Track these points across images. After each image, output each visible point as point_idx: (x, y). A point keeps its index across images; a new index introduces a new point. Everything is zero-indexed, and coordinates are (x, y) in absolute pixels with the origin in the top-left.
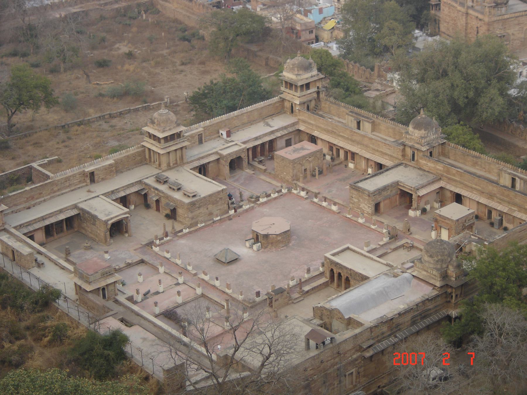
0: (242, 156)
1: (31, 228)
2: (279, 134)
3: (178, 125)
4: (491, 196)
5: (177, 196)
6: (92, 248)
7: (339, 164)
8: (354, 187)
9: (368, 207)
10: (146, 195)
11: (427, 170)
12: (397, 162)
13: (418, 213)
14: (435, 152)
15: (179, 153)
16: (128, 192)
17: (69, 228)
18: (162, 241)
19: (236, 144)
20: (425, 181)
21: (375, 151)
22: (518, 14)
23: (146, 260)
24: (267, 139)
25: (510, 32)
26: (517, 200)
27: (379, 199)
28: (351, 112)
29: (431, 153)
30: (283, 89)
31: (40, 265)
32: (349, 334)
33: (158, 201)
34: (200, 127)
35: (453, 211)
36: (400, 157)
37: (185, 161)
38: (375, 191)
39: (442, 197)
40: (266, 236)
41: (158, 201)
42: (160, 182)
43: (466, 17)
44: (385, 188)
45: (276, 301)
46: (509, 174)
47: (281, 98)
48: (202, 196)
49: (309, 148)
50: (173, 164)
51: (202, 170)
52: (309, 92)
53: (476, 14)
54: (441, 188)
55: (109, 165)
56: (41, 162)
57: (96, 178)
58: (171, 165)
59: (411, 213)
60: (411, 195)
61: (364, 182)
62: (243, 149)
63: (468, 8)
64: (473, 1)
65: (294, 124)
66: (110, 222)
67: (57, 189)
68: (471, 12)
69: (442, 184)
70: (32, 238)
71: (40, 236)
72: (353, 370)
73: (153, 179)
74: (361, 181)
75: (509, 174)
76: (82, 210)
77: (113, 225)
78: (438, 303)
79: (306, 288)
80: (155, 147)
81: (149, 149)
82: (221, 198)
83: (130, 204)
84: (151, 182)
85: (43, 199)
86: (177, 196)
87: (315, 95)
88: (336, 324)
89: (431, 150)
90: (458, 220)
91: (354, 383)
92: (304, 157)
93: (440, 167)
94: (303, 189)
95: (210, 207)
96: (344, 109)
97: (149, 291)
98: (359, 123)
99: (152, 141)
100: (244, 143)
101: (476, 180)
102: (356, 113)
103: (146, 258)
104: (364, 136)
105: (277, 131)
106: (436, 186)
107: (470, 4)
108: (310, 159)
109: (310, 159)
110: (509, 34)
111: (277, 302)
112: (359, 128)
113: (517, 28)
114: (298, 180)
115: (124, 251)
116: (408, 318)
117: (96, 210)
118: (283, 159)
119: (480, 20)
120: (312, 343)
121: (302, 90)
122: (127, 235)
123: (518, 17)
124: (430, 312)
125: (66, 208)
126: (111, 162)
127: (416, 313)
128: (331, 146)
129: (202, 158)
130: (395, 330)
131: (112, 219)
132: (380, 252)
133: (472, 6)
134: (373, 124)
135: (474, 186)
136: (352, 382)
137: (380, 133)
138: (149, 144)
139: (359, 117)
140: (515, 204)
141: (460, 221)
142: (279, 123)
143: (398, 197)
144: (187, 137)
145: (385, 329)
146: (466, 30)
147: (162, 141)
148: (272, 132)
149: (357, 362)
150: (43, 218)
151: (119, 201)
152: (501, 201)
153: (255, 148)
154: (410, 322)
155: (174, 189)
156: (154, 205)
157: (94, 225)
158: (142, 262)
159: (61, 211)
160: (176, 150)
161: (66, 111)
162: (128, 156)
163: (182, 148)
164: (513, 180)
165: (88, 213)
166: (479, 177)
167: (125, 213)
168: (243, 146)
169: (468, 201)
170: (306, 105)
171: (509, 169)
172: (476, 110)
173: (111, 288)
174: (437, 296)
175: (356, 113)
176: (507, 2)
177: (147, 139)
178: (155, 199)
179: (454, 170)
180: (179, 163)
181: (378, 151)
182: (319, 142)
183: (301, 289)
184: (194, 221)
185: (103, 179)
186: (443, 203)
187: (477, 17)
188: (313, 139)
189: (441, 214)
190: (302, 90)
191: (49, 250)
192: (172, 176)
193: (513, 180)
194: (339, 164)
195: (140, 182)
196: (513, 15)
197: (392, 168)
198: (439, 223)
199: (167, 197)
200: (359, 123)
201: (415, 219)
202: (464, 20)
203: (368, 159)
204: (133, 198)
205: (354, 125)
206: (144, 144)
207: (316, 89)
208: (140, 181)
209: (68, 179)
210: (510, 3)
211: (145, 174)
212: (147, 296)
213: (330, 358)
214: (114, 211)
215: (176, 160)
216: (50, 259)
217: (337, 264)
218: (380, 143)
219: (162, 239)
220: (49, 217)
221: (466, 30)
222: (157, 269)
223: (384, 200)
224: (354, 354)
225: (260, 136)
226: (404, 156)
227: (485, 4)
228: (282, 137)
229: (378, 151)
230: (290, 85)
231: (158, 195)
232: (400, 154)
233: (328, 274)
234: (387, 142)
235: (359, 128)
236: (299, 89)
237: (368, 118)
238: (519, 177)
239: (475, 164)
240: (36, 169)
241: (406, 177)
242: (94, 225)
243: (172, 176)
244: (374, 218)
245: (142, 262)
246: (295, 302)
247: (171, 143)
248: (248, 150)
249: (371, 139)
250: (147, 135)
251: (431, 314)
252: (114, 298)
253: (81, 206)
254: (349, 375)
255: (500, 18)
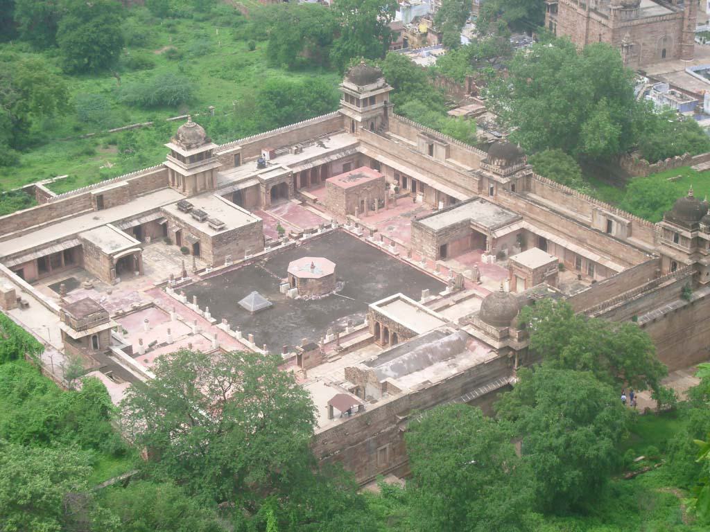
0: (288, 183)
1: (19, 261)
2: (334, 157)
3: (207, 142)
4: (581, 242)
5: (203, 227)
6: (93, 287)
7: (406, 196)
8: (417, 225)
9: (431, 250)
10: (165, 225)
11: (507, 207)
12: (472, 196)
13: (492, 258)
14: (519, 187)
15: (208, 177)
16: (143, 220)
17: (62, 265)
18: (179, 282)
19: (281, 167)
20: (503, 220)
21: (447, 182)
22: (651, 20)
23: (157, 304)
24: (319, 162)
25: (641, 41)
26: (611, 248)
27: (446, 240)
28: (423, 133)
29: (513, 187)
30: (342, 102)
31: (25, 306)
32: (382, 402)
33: (178, 234)
34: (237, 144)
35: (533, 258)
36: (476, 191)
37: (215, 186)
38: (441, 231)
39: (522, 240)
40: (304, 280)
41: (178, 234)
42: (182, 211)
43: (588, 22)
44: (453, 227)
45: (305, 359)
46: (605, 215)
47: (340, 113)
48: (231, 228)
49: (368, 175)
50: (201, 189)
51: (238, 198)
52: (374, 107)
53: (599, 18)
54: (523, 230)
55: (121, 187)
56: (48, 181)
57: (105, 202)
58: (199, 189)
59: (484, 258)
60: (486, 236)
61: (429, 219)
62: (289, 173)
63: (590, 10)
64: (596, 2)
65: (354, 146)
66: (116, 257)
67: (55, 214)
68: (593, 15)
69: (524, 224)
70: (20, 273)
71: (31, 271)
72: (387, 445)
73: (175, 206)
74: (426, 217)
75: (605, 215)
76: (85, 240)
77: (121, 260)
78: (497, 368)
79: (345, 344)
80: (180, 169)
81: (173, 171)
82: (254, 233)
83: (145, 236)
84: (172, 210)
85: (37, 226)
86: (203, 227)
87: (382, 112)
88: (371, 390)
89: (513, 183)
90: (536, 269)
91: (388, 461)
92: (361, 186)
93: (522, 204)
94: (357, 225)
95: (241, 242)
96: (415, 130)
97: (156, 342)
98: (431, 147)
99: (175, 160)
100: (290, 166)
101: (564, 221)
102: (429, 136)
103: (156, 301)
104: (436, 163)
105: (333, 153)
106: (515, 227)
107: (593, 5)
108: (368, 189)
109: (368, 189)
110: (638, 44)
111: (308, 361)
112: (431, 153)
113: (649, 37)
114: (353, 214)
115: (131, 291)
116: (459, 384)
117: (101, 242)
118: (336, 188)
119: (604, 25)
120: (336, 412)
121: (365, 105)
122: (137, 273)
123: (651, 23)
124: (485, 379)
125: (64, 238)
126: (124, 183)
127: (469, 380)
128: (397, 175)
129: (238, 182)
130: (440, 399)
131: (119, 252)
132: (438, 305)
133: (596, 9)
134: (448, 148)
135: (560, 229)
136: (385, 460)
137: (456, 159)
138: (172, 164)
139: (432, 140)
140: (607, 253)
141: (539, 270)
142: (338, 142)
143: (470, 238)
144: (219, 156)
145: (428, 397)
146: (587, 37)
147: (188, 161)
148: (327, 155)
149: (391, 436)
150: (36, 249)
151: (132, 231)
152: (592, 248)
153: (304, 173)
154: (460, 391)
155: (198, 220)
156: (174, 238)
157: (98, 259)
158: (152, 305)
159: (58, 242)
160: (204, 172)
161: (227, 107)
162: (146, 177)
163: (212, 170)
164: (609, 224)
165: (91, 244)
166: (567, 217)
167: (136, 247)
168: (289, 170)
169: (553, 247)
170: (370, 124)
171: (605, 208)
172: (590, 138)
173: (102, 336)
174: (495, 360)
175: (429, 136)
176: (639, 4)
177: (169, 157)
178: (175, 231)
179: (537, 208)
180: (207, 185)
181: (450, 182)
182: (383, 169)
183: (338, 345)
184: (219, 259)
185: (113, 205)
186: (524, 247)
187: (600, 22)
188: (376, 165)
189: (518, 261)
190: (365, 105)
191: (41, 291)
192: (197, 203)
193: (609, 224)
194: (406, 196)
195: (157, 210)
196: (645, 21)
197: (466, 203)
198: (513, 271)
199: (190, 228)
200: (431, 147)
201: (488, 266)
202: (585, 25)
203: (439, 192)
204: (150, 229)
205: (425, 150)
206: (166, 163)
207: (382, 104)
208: (159, 208)
209: (69, 203)
210: (642, 5)
211: (166, 199)
212: (153, 347)
213: (356, 430)
214: (127, 243)
215: (205, 184)
216: (37, 298)
217: (383, 317)
218: (453, 172)
219: (179, 279)
220: (44, 248)
221: (587, 37)
222: (166, 314)
223: (453, 241)
224: (388, 425)
225: (311, 159)
226: (480, 189)
227: (610, 6)
228: (338, 160)
229: (450, 182)
230: (351, 98)
231: (178, 226)
232: (476, 186)
233: (373, 329)
234: (462, 171)
235: (431, 153)
236: (361, 104)
237: (442, 141)
238: (616, 220)
239: (564, 202)
240: (40, 189)
241: (482, 214)
242: (98, 259)
243: (197, 203)
244: (441, 262)
245: (152, 305)
246: (330, 360)
247: (199, 163)
248: (295, 175)
249: (443, 167)
250: (170, 152)
251: (488, 381)
252: (108, 349)
253: (83, 236)
254: (381, 451)
255: (629, 23)
